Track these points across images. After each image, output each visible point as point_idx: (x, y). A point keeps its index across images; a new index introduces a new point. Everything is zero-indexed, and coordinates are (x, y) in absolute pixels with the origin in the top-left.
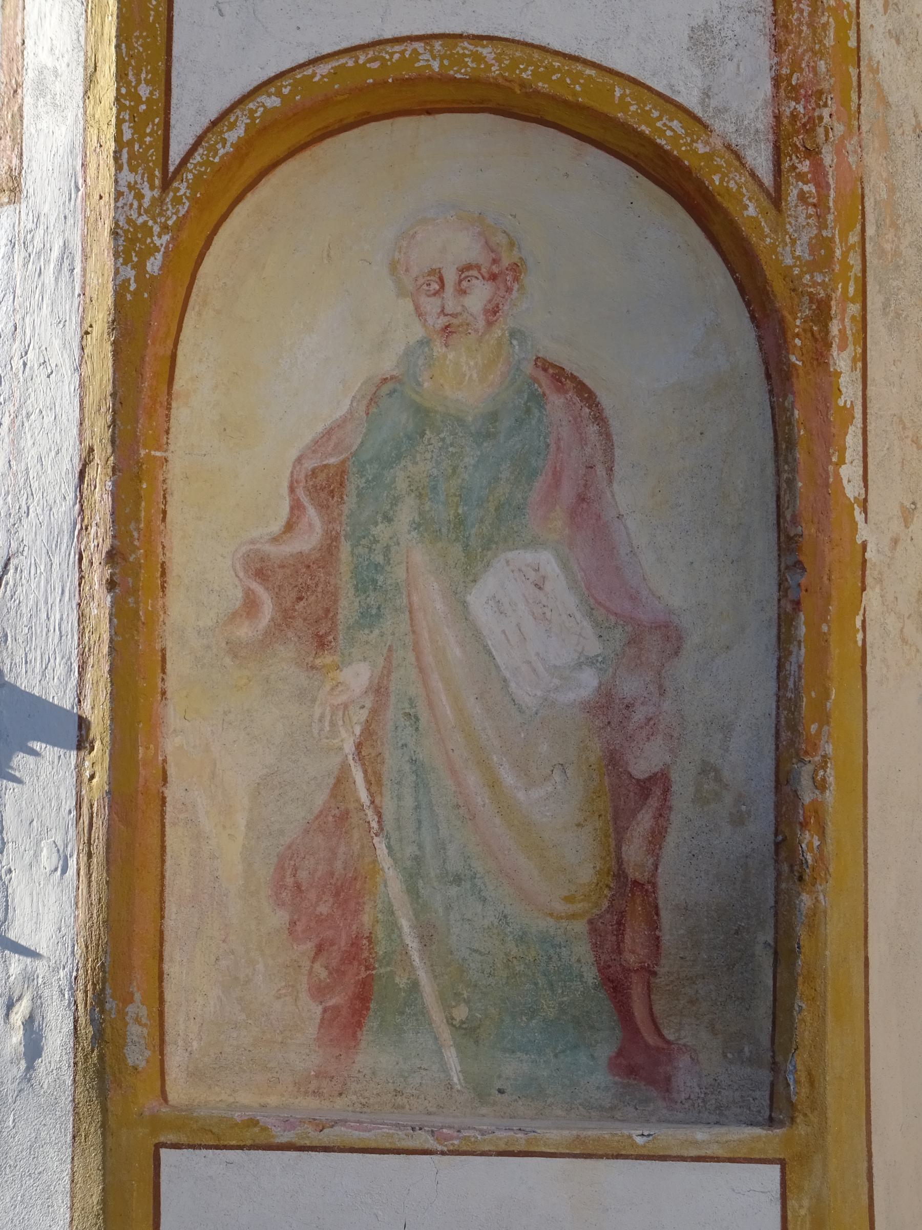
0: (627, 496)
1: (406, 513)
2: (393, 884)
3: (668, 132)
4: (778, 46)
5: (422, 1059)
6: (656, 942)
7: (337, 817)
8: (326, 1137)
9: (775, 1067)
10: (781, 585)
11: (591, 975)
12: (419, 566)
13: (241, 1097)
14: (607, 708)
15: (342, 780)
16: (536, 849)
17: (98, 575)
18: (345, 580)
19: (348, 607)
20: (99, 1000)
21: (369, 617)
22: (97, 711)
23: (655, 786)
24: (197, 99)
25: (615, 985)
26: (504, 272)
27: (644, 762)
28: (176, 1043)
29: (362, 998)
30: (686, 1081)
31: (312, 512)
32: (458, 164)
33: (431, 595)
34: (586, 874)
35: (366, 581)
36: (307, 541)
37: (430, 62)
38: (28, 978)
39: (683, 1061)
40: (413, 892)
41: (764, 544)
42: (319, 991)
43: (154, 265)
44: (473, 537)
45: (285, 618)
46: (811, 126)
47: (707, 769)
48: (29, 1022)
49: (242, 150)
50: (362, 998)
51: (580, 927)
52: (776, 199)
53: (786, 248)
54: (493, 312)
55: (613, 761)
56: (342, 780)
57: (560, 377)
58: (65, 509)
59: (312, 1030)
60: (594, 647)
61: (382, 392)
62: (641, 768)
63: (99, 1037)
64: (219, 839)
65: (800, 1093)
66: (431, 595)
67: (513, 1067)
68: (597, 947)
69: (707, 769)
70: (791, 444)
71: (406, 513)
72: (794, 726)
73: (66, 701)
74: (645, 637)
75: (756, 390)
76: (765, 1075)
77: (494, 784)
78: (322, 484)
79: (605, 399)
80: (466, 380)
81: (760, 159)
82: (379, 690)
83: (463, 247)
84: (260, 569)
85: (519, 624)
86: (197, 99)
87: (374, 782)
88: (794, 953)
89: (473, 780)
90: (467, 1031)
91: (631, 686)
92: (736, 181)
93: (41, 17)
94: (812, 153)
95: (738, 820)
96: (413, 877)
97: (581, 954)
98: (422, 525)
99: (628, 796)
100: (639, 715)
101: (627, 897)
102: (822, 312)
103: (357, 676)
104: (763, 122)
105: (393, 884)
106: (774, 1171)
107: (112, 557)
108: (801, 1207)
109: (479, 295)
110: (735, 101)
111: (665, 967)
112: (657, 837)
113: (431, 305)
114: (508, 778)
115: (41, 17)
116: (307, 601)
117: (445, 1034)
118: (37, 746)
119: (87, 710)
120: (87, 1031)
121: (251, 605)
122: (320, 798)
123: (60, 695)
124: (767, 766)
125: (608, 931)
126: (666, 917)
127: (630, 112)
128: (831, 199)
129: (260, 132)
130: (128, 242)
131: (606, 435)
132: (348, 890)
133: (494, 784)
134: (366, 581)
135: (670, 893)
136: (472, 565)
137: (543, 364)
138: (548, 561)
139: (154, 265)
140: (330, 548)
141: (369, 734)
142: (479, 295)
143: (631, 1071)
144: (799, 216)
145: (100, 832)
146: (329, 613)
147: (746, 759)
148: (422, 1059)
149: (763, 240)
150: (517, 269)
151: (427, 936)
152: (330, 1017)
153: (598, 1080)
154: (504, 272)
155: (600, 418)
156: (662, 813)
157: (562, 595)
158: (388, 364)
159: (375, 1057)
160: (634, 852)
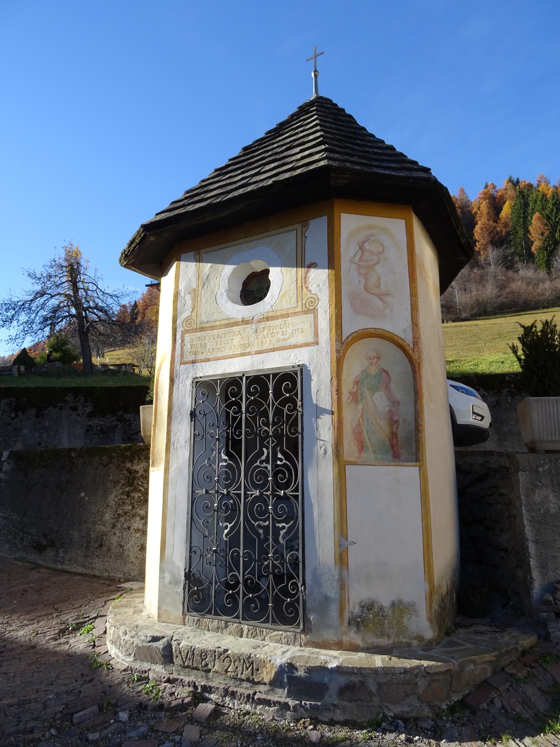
0: (393, 386)
1: (366, 387)
2: (365, 433)
3: (401, 342)
4: (413, 332)
5: (369, 455)
6: (397, 441)
7: (359, 424)
8: (366, 463)
9: (416, 455)
10: (415, 397)
11: (389, 445)
12: (367, 393)
13: (353, 459)
14: (390, 412)
15: (359, 420)
16: (380, 430)
17: (334, 393)
18: (359, 395)
19: (359, 398)
20: (337, 446)
21: (362, 400)
22: (335, 409)
23: (397, 422)
24: (347, 332)
25: (392, 446)
26: (378, 357)
27: (395, 418)
29: (362, 447)
30: (402, 458)
31: (355, 386)
33: (368, 397)
34: (388, 432)
35: (361, 395)
36: (355, 390)
37: (373, 331)
38: (324, 444)
39: (402, 455)
40: (367, 434)
41: (412, 392)
42: (358, 446)
43: (341, 354)
44: (373, 390)
45: (353, 399)
46: (417, 342)
47: (404, 420)
48: (325, 450)
49: (351, 340)
50: (362, 447)
51: (387, 439)
52: (414, 351)
53: (415, 357)
54: (377, 362)
55: (391, 418)
56: (359, 420)
57: (384, 371)
58: (329, 384)
59: (357, 451)
60: (388, 404)
61: (363, 371)
62: (395, 419)
63: (337, 451)
64: (348, 427)
65: (421, 458)
66: (368, 397)
67: (380, 456)
68: (390, 441)
69: (404, 420)
70: (416, 380)
71: (366, 387)
72: (418, 414)
73: (330, 409)
74: (395, 403)
75: (411, 374)
76: (415, 456)
77: (376, 421)
78: (357, 383)
79: (390, 374)
80: (373, 371)
81: (412, 346)
82: (363, 409)
83: (374, 354)
84: (350, 393)
85: (379, 401)
86: (347, 332)
87: (363, 420)
88: (419, 441)
89: (374, 420)
90: (374, 452)
91: (393, 409)
92: (409, 348)
93: (321, 322)
94: (417, 345)
95: (409, 425)
96: (367, 432)
97: (388, 442)
98: (368, 388)
99: (393, 423)
100: (394, 413)
101: (393, 435)
102: (419, 364)
103: (360, 407)
104: (412, 341)
105: (365, 433)
106: (418, 468)
107: (337, 391)
108: (421, 472)
109: (375, 360)
110: (408, 338)
112: (397, 428)
113: (370, 361)
114: (378, 420)
115: (321, 322)
116: (355, 397)
117: (372, 452)
119: (333, 410)
120: (335, 450)
121: (349, 397)
122: (357, 422)
123: (328, 407)
124: (414, 419)
125: (391, 440)
126: (399, 438)
127: (396, 339)
129: (353, 338)
130: (338, 351)
131: (390, 378)
132: (360, 433)
133: (376, 421)
134: (361, 395)
135: (399, 435)
136: (373, 394)
137: (382, 369)
138: (382, 393)
139: (341, 354)
140: (357, 391)
141: (362, 415)
142: (375, 360)
143: (395, 457)
144: (416, 353)
145: (336, 425)
146: (357, 399)
147: (410, 418)
148: (369, 455)
149: (412, 355)
150: (380, 357)
151: (369, 439)
152: (359, 450)
154: (378, 357)
155: (389, 376)
156: (398, 425)
157: (384, 398)
158: (364, 368)
159: (364, 455)
160: (394, 430)
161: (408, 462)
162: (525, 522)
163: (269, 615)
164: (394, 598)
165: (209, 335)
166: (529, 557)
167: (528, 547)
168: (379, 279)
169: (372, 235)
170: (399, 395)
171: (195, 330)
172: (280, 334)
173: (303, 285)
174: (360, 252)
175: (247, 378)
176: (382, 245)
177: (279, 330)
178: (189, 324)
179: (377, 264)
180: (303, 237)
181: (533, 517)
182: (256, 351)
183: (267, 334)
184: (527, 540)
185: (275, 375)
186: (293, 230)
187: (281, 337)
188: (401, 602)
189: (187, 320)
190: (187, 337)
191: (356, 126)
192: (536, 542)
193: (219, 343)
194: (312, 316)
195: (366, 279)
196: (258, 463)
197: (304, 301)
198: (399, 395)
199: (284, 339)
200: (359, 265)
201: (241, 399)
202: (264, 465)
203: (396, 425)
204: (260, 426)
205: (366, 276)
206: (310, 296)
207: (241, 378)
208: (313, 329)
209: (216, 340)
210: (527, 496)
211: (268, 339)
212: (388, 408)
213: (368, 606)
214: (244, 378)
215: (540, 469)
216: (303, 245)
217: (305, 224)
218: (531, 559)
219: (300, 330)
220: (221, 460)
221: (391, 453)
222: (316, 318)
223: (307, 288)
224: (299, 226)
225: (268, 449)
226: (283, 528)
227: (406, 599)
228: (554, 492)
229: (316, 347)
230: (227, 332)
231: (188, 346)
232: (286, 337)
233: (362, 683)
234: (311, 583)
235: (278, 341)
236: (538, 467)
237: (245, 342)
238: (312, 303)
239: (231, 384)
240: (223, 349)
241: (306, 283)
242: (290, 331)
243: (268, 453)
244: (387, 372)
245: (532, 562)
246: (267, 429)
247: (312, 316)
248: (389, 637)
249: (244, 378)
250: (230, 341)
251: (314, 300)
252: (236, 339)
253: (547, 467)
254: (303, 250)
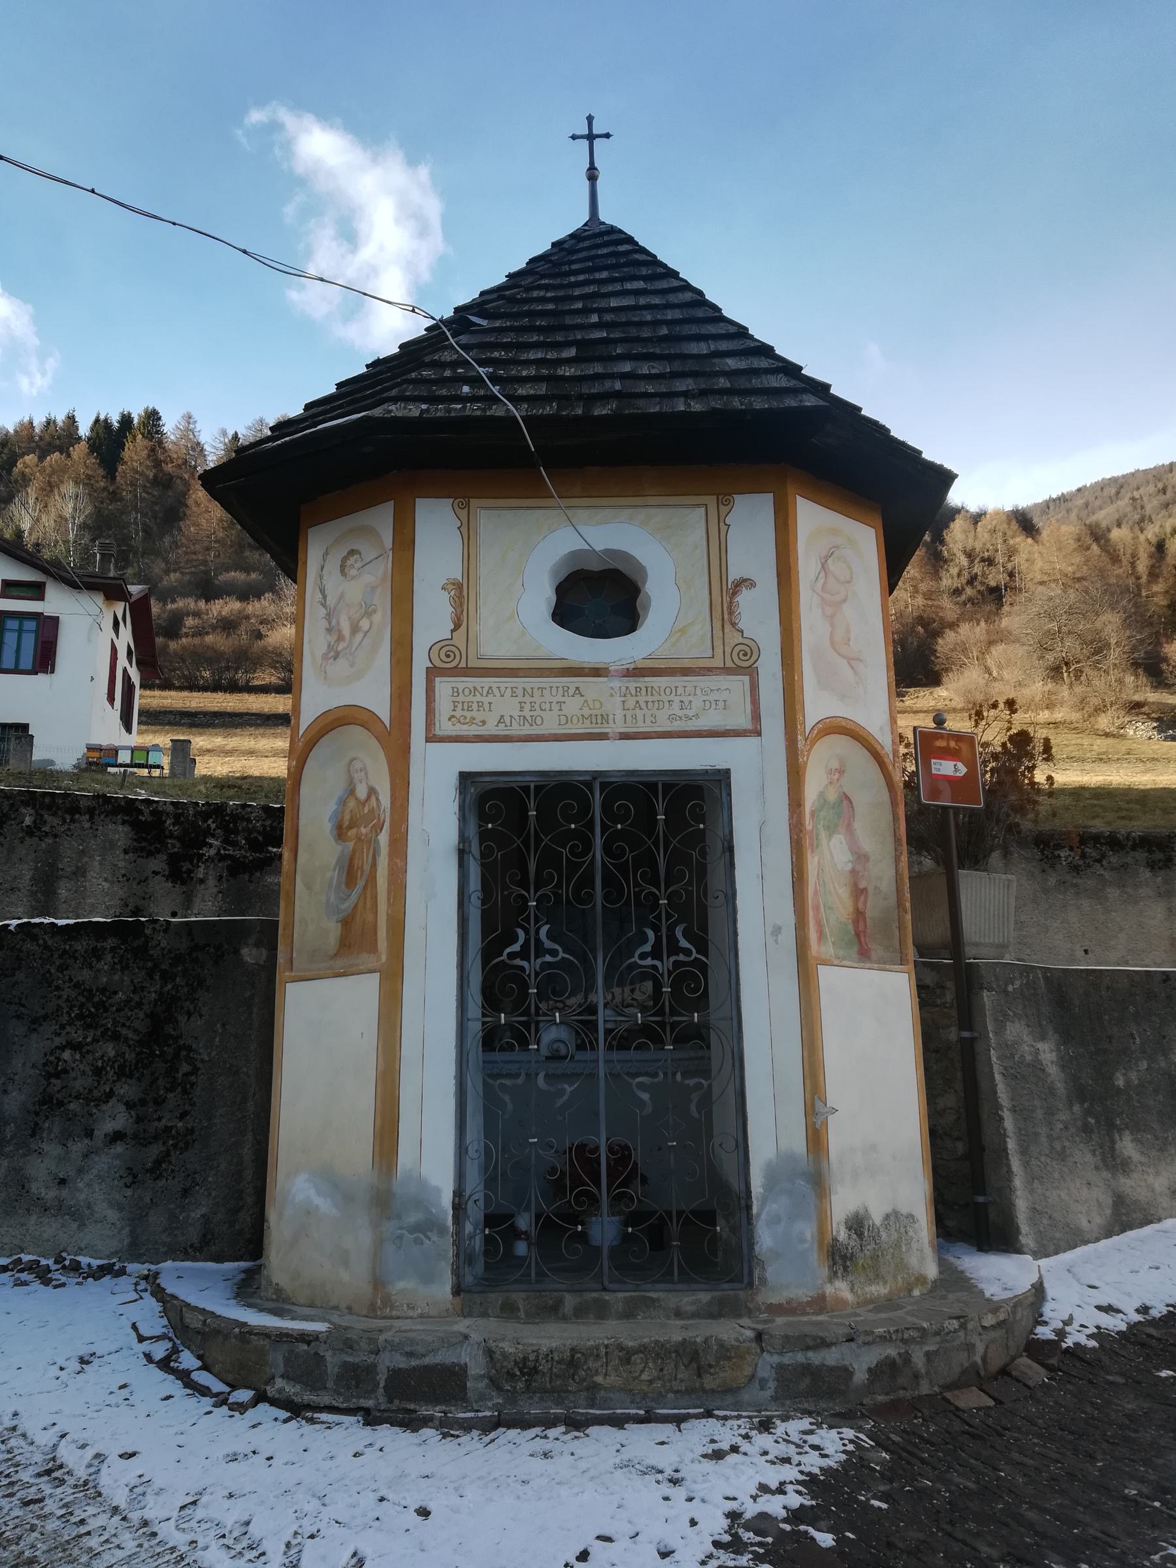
0: (857, 825)
3: (878, 748)
10: (896, 850)
14: (853, 872)
23: (864, 891)
25: (857, 935)
26: (841, 772)
27: (862, 885)
28: (405, 408)
30: (874, 956)
32: (839, 745)
34: (851, 910)
35: (818, 835)
47: (876, 888)
55: (855, 885)
57: (847, 798)
62: (861, 886)
66: (824, 841)
74: (860, 857)
76: (899, 955)
80: (832, 796)
81: (891, 756)
90: (834, 943)
91: (858, 868)
95: (885, 899)
97: (851, 927)
99: (858, 892)
101: (859, 915)
111: (868, 931)
112: (865, 902)
118: (1093, 1343)
124: (894, 889)
125: (856, 922)
128: (42, 920)
135: (868, 914)
136: (830, 836)
138: (842, 836)
153: (855, 955)
156: (866, 897)
160: (860, 905)
161: (884, 963)
162: (998, 1077)
163: (672, 1262)
164: (888, 1209)
165: (503, 686)
166: (1005, 1136)
167: (1002, 1119)
168: (848, 631)
169: (837, 547)
170: (868, 844)
171: (468, 672)
172: (676, 705)
173: (726, 616)
174: (823, 574)
175: (603, 786)
176: (849, 568)
177: (672, 697)
178: (448, 656)
179: (844, 601)
180: (722, 524)
181: (1005, 1068)
182: (621, 733)
183: (647, 702)
184: (999, 1107)
185: (667, 787)
186: (698, 506)
187: (681, 713)
188: (896, 1213)
189: (444, 647)
190: (444, 686)
191: (721, 329)
192: (1013, 1110)
193: (527, 707)
194: (746, 679)
195: (832, 625)
196: (636, 959)
197: (728, 650)
198: (868, 844)
199: (687, 717)
200: (823, 599)
201: (590, 825)
202: (649, 961)
203: (862, 898)
204: (636, 884)
205: (831, 619)
206: (741, 640)
207: (589, 785)
208: (749, 706)
209: (520, 699)
210: (996, 1033)
211: (648, 713)
212: (850, 866)
213: (857, 1224)
214: (597, 786)
215: (1010, 988)
216: (723, 540)
217: (725, 497)
218: (1008, 1140)
219: (721, 704)
220: (540, 951)
221: (856, 948)
222: (754, 687)
223: (734, 624)
224: (711, 500)
225: (656, 929)
226: (643, 956)
227: (904, 1210)
228: (1028, 1026)
229: (754, 740)
230: (547, 686)
231: (443, 705)
232: (691, 713)
233: (906, 1358)
234: (762, 1190)
235: (672, 718)
236: (1006, 985)
237: (594, 712)
238: (745, 655)
239: (562, 791)
240: (539, 721)
241: (731, 613)
242: (697, 703)
243: (658, 939)
244: (850, 802)
245: (1011, 1145)
246: (655, 890)
247: (746, 679)
248: (885, 1283)
249: (597, 786)
250: (555, 707)
251: (750, 651)
252: (565, 704)
253: (1017, 984)
254: (723, 550)
